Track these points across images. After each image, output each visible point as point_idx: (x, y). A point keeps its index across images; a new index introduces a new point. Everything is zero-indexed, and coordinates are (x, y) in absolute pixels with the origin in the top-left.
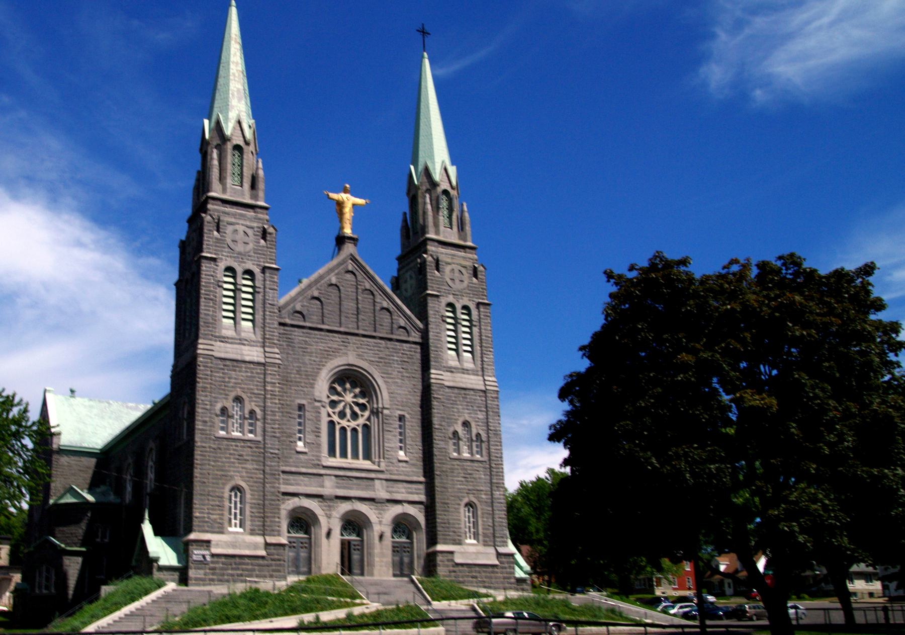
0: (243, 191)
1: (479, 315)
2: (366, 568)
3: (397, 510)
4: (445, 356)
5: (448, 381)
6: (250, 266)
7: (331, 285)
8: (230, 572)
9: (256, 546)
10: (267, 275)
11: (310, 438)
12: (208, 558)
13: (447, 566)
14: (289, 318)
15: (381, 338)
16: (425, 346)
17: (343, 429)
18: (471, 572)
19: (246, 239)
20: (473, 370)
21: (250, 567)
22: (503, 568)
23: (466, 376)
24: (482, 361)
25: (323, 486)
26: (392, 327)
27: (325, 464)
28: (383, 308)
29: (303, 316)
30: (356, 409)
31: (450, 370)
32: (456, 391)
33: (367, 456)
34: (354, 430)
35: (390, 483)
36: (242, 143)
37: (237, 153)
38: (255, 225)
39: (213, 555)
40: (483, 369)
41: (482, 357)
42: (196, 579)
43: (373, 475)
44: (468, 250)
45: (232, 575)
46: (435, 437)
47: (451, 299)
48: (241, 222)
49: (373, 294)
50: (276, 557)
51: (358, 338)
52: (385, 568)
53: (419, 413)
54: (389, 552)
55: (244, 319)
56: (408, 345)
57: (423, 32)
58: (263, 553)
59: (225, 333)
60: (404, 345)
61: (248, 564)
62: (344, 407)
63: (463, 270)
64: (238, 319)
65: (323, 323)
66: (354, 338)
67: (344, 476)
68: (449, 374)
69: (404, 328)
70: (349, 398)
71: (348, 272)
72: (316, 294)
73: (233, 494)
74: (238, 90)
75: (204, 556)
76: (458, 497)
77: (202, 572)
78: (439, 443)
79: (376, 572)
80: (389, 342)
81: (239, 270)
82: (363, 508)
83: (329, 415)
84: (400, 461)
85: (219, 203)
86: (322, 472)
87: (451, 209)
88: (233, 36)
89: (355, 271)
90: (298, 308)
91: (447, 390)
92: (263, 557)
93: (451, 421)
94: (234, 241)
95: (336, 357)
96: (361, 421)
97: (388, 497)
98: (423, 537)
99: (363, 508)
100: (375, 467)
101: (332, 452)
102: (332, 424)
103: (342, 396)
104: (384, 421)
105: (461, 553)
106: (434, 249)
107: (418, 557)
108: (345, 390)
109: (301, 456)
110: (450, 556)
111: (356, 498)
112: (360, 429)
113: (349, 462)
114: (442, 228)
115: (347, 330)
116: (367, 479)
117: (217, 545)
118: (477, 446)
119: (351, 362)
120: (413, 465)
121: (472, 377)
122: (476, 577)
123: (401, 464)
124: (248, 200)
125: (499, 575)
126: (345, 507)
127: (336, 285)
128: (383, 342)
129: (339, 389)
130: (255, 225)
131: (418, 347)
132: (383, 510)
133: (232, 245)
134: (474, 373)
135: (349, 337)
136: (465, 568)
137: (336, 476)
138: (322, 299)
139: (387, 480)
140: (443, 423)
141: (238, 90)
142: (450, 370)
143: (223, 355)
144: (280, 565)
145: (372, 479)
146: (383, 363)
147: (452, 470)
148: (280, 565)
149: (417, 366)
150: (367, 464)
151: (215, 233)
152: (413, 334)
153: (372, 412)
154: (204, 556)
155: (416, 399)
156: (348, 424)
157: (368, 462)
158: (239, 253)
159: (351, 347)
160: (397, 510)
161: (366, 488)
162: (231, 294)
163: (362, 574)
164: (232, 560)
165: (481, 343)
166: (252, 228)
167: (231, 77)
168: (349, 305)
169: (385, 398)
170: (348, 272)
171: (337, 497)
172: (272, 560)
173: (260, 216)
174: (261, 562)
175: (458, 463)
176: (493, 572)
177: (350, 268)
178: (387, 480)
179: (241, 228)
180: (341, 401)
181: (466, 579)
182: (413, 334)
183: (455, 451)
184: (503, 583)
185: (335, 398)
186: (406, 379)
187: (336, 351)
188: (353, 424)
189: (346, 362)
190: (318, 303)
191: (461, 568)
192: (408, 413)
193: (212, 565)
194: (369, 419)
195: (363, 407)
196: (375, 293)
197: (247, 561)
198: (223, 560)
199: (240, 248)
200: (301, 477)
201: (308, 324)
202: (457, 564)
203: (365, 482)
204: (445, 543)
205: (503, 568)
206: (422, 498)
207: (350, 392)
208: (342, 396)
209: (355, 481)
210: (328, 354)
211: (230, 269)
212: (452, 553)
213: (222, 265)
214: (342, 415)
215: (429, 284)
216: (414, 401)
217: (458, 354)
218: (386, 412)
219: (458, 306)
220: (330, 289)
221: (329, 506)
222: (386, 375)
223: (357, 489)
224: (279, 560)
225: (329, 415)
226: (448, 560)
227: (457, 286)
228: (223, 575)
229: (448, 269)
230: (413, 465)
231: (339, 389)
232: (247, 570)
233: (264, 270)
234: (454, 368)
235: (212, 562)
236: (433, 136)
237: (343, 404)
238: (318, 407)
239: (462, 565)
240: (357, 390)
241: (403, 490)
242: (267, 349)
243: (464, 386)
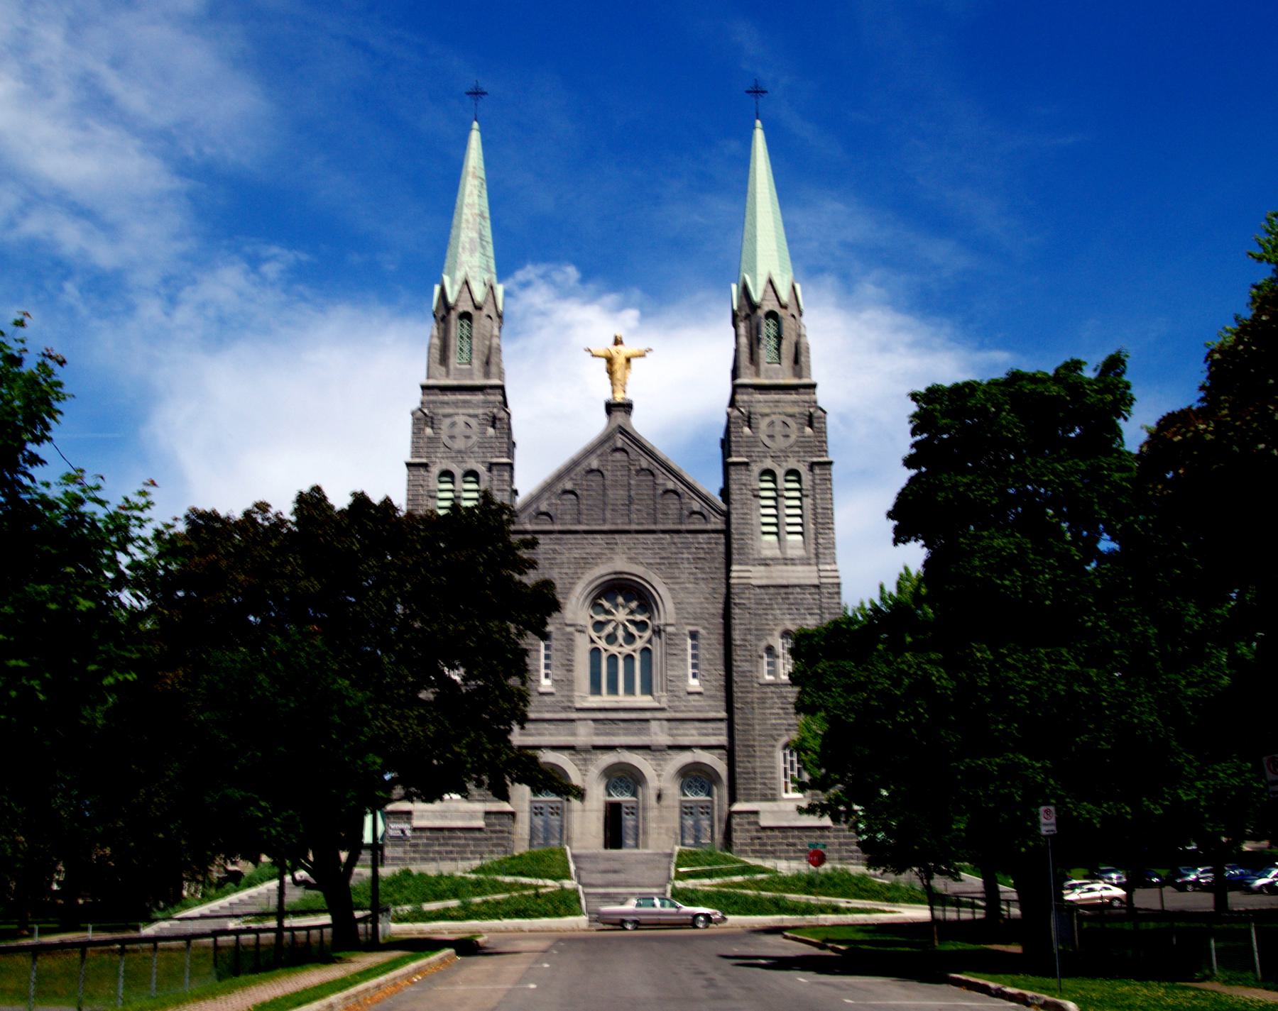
0: (471, 370)
1: (813, 481)
2: (641, 836)
3: (686, 758)
4: (756, 545)
5: (761, 578)
6: (792, 464)
7: (592, 471)
8: (437, 848)
9: (472, 815)
10: (495, 472)
11: (557, 673)
12: (408, 833)
13: (748, 831)
14: (530, 523)
15: (664, 532)
16: (727, 533)
17: (613, 658)
18: (787, 838)
19: (468, 432)
20: (801, 559)
21: (463, 842)
22: (838, 830)
23: (790, 568)
24: (817, 544)
25: (574, 734)
26: (681, 515)
27: (578, 705)
28: (667, 491)
29: (704, 517)
30: (632, 629)
31: (765, 562)
32: (772, 590)
33: (647, 689)
34: (629, 658)
35: (673, 724)
36: (470, 309)
37: (771, 321)
38: (480, 411)
39: (414, 829)
40: (817, 555)
41: (816, 539)
42: (393, 858)
43: (648, 715)
44: (802, 390)
45: (439, 852)
46: (735, 657)
47: (768, 464)
48: (461, 411)
49: (653, 474)
50: (498, 828)
51: (629, 536)
52: (664, 837)
53: (721, 626)
54: (676, 814)
55: (764, 533)
56: (705, 536)
57: (757, 91)
58: (480, 823)
59: (767, 553)
60: (700, 536)
61: (460, 838)
62: (615, 628)
63: (789, 421)
64: (782, 533)
65: (579, 523)
66: (623, 536)
67: (605, 719)
68: (762, 568)
69: (700, 513)
70: (621, 615)
71: (617, 450)
72: (569, 486)
73: (788, 752)
74: (472, 240)
75: (403, 831)
76: (772, 736)
77: (400, 849)
78: (740, 664)
79: (651, 842)
80: (675, 536)
81: (459, 473)
82: (635, 759)
83: (592, 641)
84: (690, 693)
85: (437, 391)
86: (574, 715)
87: (779, 338)
88: (470, 169)
89: (626, 448)
90: (543, 508)
91: (758, 591)
92: (480, 829)
93: (761, 632)
94: (452, 437)
95: (597, 564)
96: (639, 644)
97: (670, 743)
98: (725, 792)
99: (635, 759)
100: (656, 705)
101: (596, 688)
102: (595, 652)
103: (612, 614)
104: (672, 641)
105: (773, 812)
106: (745, 397)
107: (720, 820)
108: (616, 606)
109: (546, 698)
110: (752, 818)
111: (622, 747)
112: (637, 656)
113: (622, 699)
114: (763, 366)
115: (613, 527)
116: (639, 719)
117: (422, 817)
118: (769, 664)
119: (618, 569)
120: (711, 697)
121: (800, 568)
122: (794, 845)
123: (691, 697)
124: (479, 381)
125: (832, 840)
126: (608, 759)
127: (599, 471)
128: (667, 536)
129: (607, 605)
130: (480, 411)
131: (722, 536)
132: (665, 760)
133: (767, 441)
134: (805, 562)
135: (617, 536)
136: (777, 833)
137: (594, 720)
138: (578, 492)
139: (668, 720)
140: (749, 637)
141: (472, 240)
142: (765, 562)
143: (764, 582)
144: (503, 838)
145: (647, 720)
146: (667, 565)
147: (763, 700)
148: (503, 838)
149: (721, 560)
150: (641, 700)
151: (746, 430)
152: (713, 519)
153: (654, 631)
154: (403, 831)
155: (719, 607)
156: (620, 649)
157: (649, 698)
158: (459, 452)
159: (618, 549)
160: (686, 758)
161: (639, 732)
162: (772, 503)
163: (637, 846)
164: (440, 834)
165: (815, 518)
166: (476, 416)
167: (464, 225)
168: (617, 495)
169: (667, 612)
170: (617, 450)
171: (596, 748)
172: (492, 832)
173: (491, 398)
174: (477, 835)
175: (773, 689)
176: (822, 837)
177: (619, 444)
178: (668, 720)
179: (460, 420)
180: (609, 621)
181: (778, 848)
182: (713, 519)
183: (769, 673)
184: (838, 851)
185: (601, 618)
186: (701, 582)
187: (599, 556)
188: (627, 649)
189: (610, 570)
190: (573, 497)
191: (769, 833)
192: (704, 628)
193: (413, 841)
194: (650, 641)
195: (642, 626)
196: (656, 472)
197: (459, 834)
198: (428, 834)
199: (459, 444)
200: (546, 725)
201: (557, 527)
202: (764, 829)
203: (637, 725)
204: (747, 800)
205: (838, 830)
206: (723, 740)
207: (624, 607)
208: (612, 614)
209: (622, 725)
210: (585, 563)
211: (769, 472)
212: (756, 813)
213: (435, 470)
214: (611, 639)
215: (734, 449)
216: (713, 611)
217: (779, 540)
218: (669, 629)
219: (780, 473)
220: (590, 477)
221: (585, 760)
222: (670, 579)
223: (625, 735)
224: (502, 832)
225: (592, 641)
226: (749, 823)
227: (780, 443)
228: (427, 852)
229: (763, 424)
230: (711, 697)
231: (607, 605)
232: (458, 845)
233: (491, 466)
234: (772, 559)
235: (414, 838)
236: (759, 238)
237: (613, 624)
238: (572, 634)
239: (772, 829)
240: (634, 605)
241: (694, 732)
242: (821, 567)
243: (784, 582)
